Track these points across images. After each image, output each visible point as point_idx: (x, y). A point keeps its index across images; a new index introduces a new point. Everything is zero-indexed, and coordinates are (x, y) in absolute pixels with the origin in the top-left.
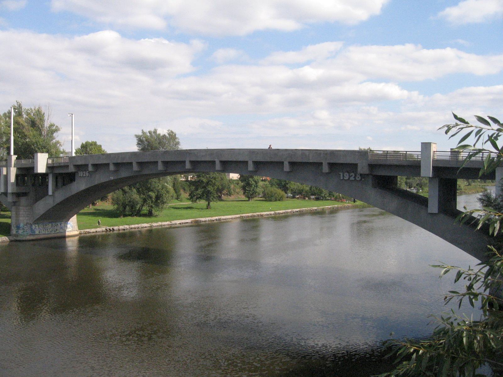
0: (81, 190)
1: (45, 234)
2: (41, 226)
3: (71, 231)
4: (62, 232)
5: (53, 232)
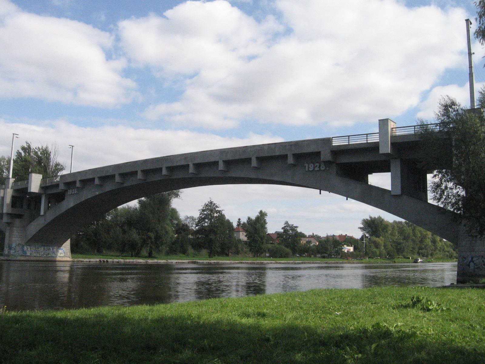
1: (36, 257)
2: (33, 249)
3: (63, 257)
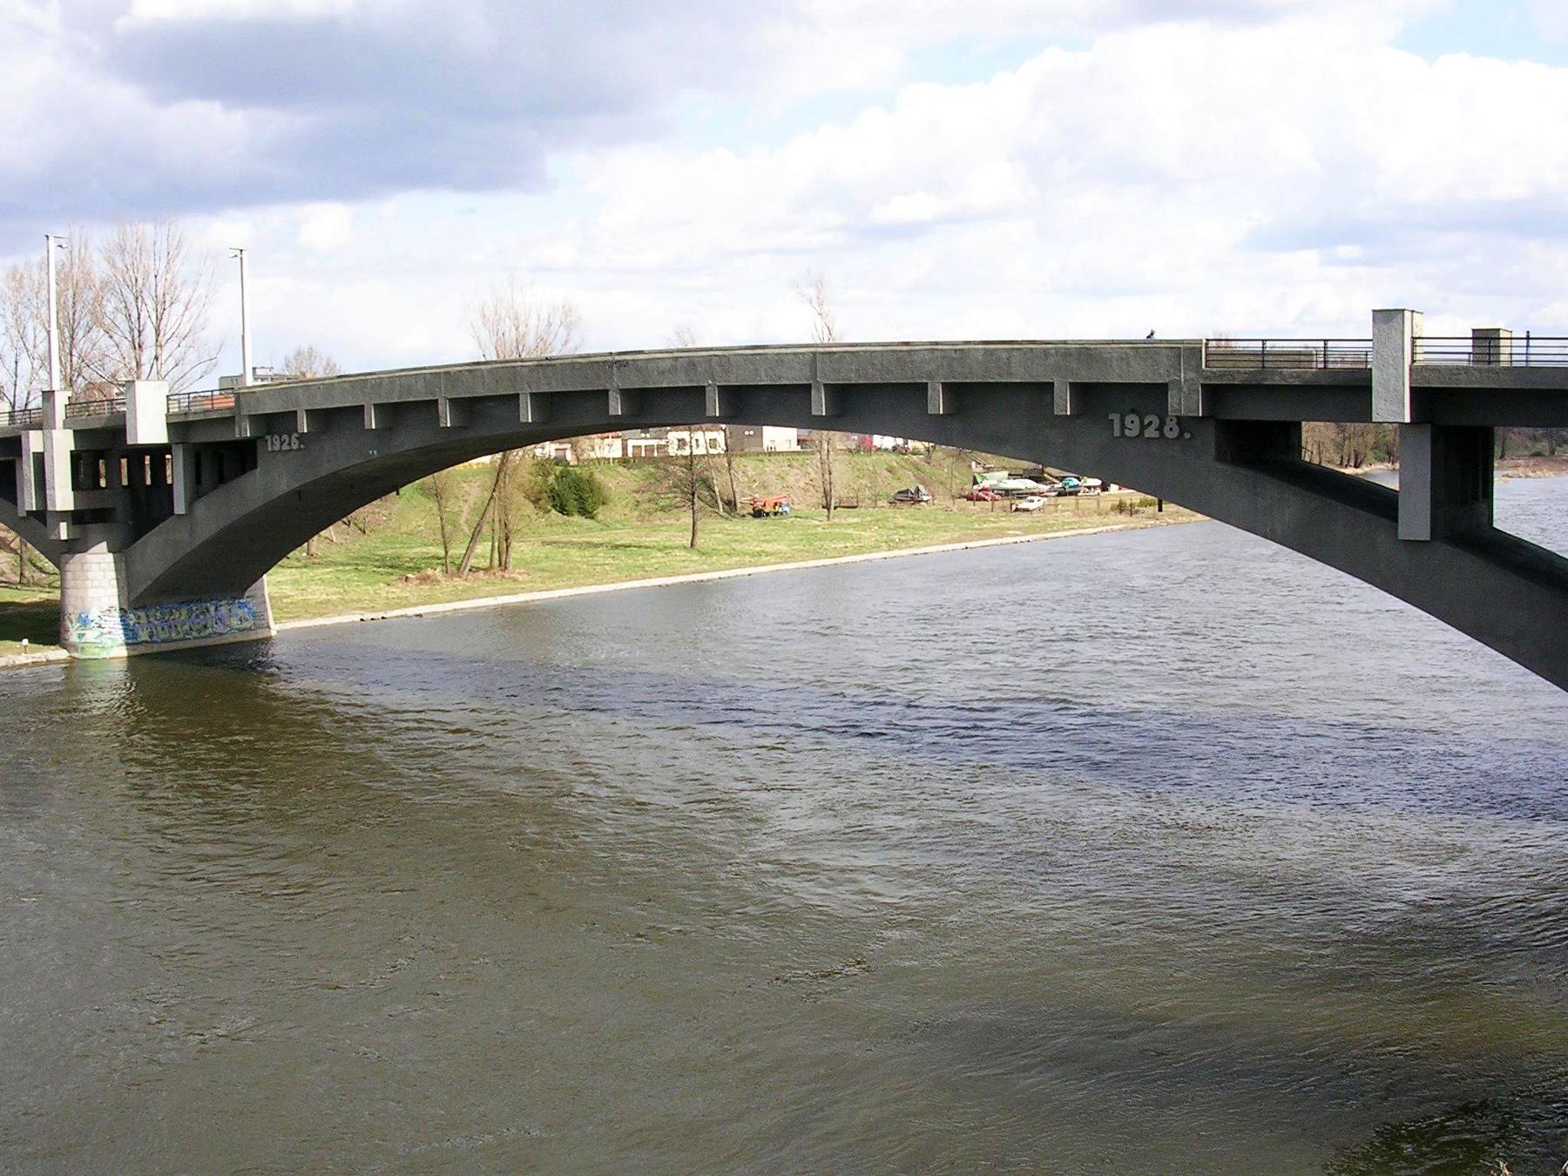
0: (276, 496)
4: (221, 634)
5: (195, 634)
